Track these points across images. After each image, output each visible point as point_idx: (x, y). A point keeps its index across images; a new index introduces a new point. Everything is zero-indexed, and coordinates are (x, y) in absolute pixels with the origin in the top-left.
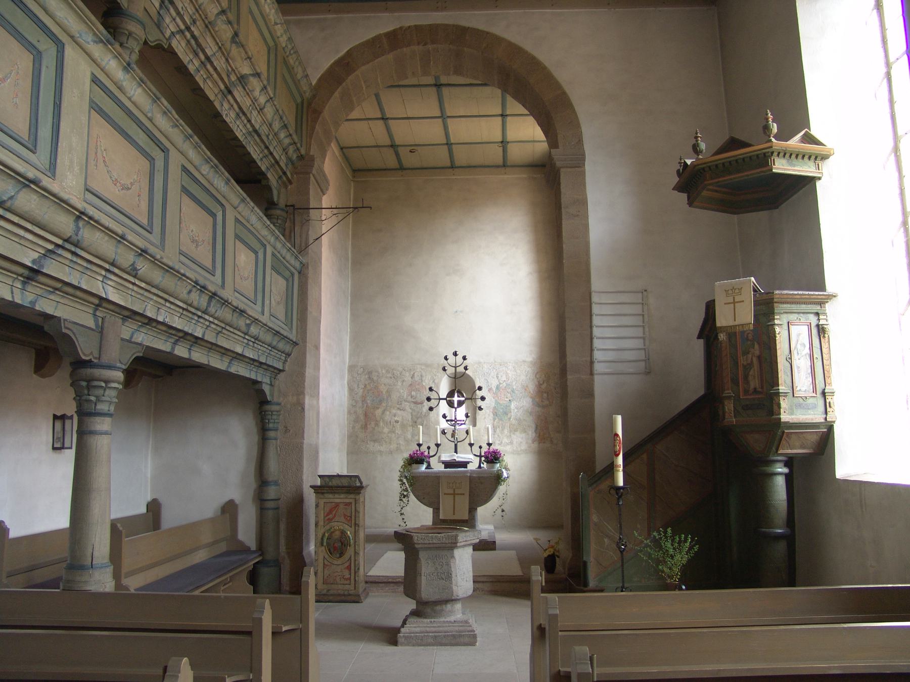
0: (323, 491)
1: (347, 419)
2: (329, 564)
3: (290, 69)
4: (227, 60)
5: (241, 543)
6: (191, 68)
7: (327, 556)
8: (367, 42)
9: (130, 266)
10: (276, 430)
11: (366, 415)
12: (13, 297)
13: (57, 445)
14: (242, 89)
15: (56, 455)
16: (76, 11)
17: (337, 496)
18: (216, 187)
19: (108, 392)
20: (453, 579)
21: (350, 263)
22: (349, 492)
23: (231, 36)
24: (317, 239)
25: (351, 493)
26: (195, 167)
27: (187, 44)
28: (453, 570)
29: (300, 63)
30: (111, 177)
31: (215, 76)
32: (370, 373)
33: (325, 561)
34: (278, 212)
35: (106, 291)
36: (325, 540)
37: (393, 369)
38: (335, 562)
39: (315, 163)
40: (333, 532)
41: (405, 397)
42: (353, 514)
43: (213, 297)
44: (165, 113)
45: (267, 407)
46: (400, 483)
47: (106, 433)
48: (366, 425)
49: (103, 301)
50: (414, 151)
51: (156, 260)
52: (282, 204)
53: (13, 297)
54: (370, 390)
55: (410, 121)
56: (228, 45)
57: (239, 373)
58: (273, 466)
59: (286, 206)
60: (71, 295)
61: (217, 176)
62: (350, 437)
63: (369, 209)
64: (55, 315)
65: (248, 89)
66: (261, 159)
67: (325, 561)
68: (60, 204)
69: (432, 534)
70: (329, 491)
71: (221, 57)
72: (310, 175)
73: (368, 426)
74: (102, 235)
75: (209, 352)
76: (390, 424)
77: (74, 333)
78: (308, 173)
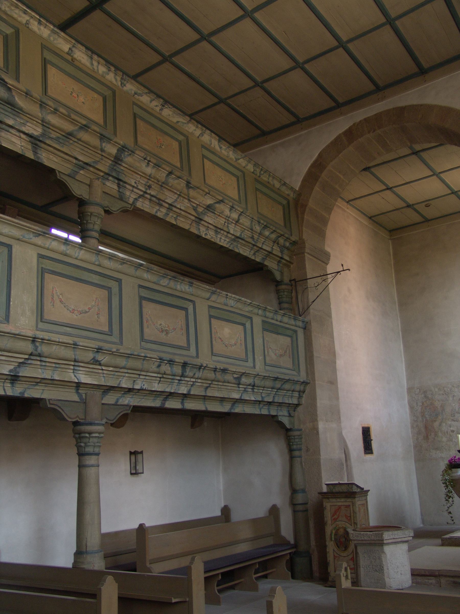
0: (328, 497)
1: (411, 432)
2: (338, 556)
3: (266, 185)
4: (189, 200)
5: (283, 538)
6: (160, 215)
7: (335, 549)
8: (332, 143)
9: (92, 359)
10: (300, 450)
11: (426, 427)
12: (5, 392)
13: (133, 471)
14: (212, 214)
15: (134, 478)
16: (15, 226)
17: (339, 500)
18: (180, 290)
19: (91, 440)
20: (385, 572)
21: (397, 306)
22: (346, 497)
23: (185, 185)
24: (313, 301)
25: (349, 498)
26: (154, 283)
27: (150, 202)
28: (384, 563)
29: (273, 178)
30: (68, 309)
31: (183, 213)
32: (425, 392)
33: (335, 553)
34: (283, 287)
35: (78, 377)
36: (333, 536)
37: (444, 387)
38: (342, 554)
39: (306, 244)
40: (338, 529)
41: (457, 409)
42: (352, 514)
43: (186, 366)
44: (110, 258)
45: (291, 433)
46: (444, 485)
47: (92, 466)
48: (427, 436)
49: (78, 385)
50: (429, 205)
51: (113, 352)
52: (286, 279)
53: (5, 392)
54: (427, 406)
55: (411, 184)
56: (185, 190)
57: (245, 412)
58: (299, 478)
59: (290, 281)
60: (51, 384)
61: (179, 283)
62: (415, 447)
63: (348, 270)
64: (41, 397)
65: (218, 212)
66: (254, 254)
67: (335, 553)
68: (15, 337)
69: (364, 533)
70: (333, 496)
71: (183, 200)
72: (304, 254)
73: (429, 437)
74: (58, 347)
75: (205, 401)
76: (448, 434)
77: (59, 407)
78: (303, 253)
